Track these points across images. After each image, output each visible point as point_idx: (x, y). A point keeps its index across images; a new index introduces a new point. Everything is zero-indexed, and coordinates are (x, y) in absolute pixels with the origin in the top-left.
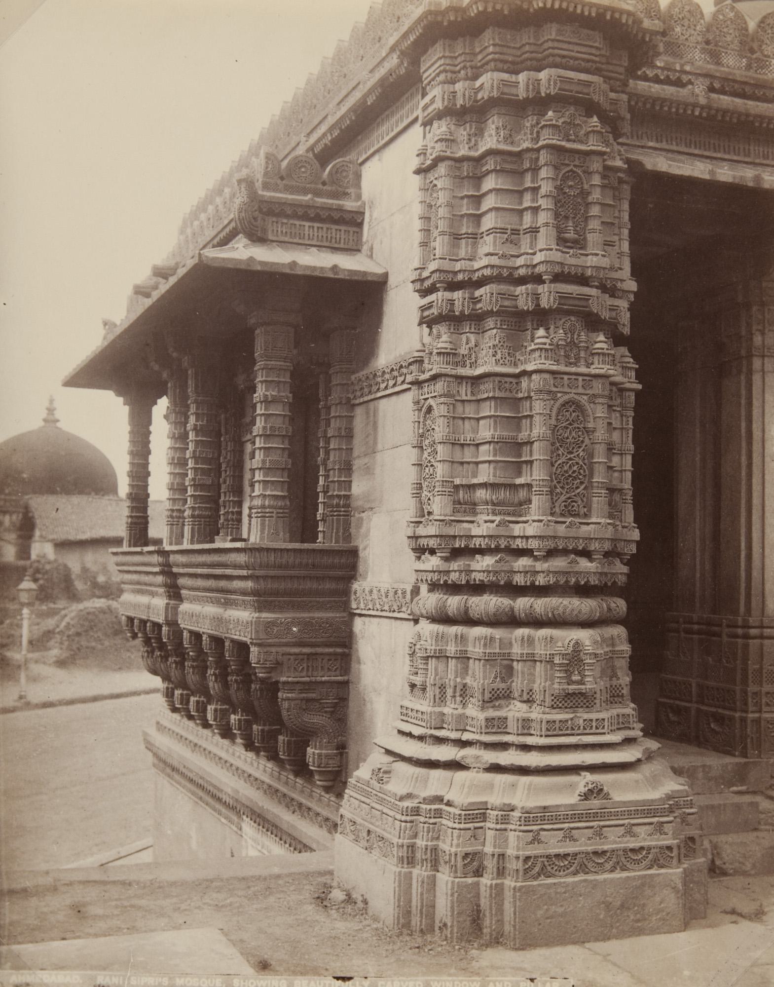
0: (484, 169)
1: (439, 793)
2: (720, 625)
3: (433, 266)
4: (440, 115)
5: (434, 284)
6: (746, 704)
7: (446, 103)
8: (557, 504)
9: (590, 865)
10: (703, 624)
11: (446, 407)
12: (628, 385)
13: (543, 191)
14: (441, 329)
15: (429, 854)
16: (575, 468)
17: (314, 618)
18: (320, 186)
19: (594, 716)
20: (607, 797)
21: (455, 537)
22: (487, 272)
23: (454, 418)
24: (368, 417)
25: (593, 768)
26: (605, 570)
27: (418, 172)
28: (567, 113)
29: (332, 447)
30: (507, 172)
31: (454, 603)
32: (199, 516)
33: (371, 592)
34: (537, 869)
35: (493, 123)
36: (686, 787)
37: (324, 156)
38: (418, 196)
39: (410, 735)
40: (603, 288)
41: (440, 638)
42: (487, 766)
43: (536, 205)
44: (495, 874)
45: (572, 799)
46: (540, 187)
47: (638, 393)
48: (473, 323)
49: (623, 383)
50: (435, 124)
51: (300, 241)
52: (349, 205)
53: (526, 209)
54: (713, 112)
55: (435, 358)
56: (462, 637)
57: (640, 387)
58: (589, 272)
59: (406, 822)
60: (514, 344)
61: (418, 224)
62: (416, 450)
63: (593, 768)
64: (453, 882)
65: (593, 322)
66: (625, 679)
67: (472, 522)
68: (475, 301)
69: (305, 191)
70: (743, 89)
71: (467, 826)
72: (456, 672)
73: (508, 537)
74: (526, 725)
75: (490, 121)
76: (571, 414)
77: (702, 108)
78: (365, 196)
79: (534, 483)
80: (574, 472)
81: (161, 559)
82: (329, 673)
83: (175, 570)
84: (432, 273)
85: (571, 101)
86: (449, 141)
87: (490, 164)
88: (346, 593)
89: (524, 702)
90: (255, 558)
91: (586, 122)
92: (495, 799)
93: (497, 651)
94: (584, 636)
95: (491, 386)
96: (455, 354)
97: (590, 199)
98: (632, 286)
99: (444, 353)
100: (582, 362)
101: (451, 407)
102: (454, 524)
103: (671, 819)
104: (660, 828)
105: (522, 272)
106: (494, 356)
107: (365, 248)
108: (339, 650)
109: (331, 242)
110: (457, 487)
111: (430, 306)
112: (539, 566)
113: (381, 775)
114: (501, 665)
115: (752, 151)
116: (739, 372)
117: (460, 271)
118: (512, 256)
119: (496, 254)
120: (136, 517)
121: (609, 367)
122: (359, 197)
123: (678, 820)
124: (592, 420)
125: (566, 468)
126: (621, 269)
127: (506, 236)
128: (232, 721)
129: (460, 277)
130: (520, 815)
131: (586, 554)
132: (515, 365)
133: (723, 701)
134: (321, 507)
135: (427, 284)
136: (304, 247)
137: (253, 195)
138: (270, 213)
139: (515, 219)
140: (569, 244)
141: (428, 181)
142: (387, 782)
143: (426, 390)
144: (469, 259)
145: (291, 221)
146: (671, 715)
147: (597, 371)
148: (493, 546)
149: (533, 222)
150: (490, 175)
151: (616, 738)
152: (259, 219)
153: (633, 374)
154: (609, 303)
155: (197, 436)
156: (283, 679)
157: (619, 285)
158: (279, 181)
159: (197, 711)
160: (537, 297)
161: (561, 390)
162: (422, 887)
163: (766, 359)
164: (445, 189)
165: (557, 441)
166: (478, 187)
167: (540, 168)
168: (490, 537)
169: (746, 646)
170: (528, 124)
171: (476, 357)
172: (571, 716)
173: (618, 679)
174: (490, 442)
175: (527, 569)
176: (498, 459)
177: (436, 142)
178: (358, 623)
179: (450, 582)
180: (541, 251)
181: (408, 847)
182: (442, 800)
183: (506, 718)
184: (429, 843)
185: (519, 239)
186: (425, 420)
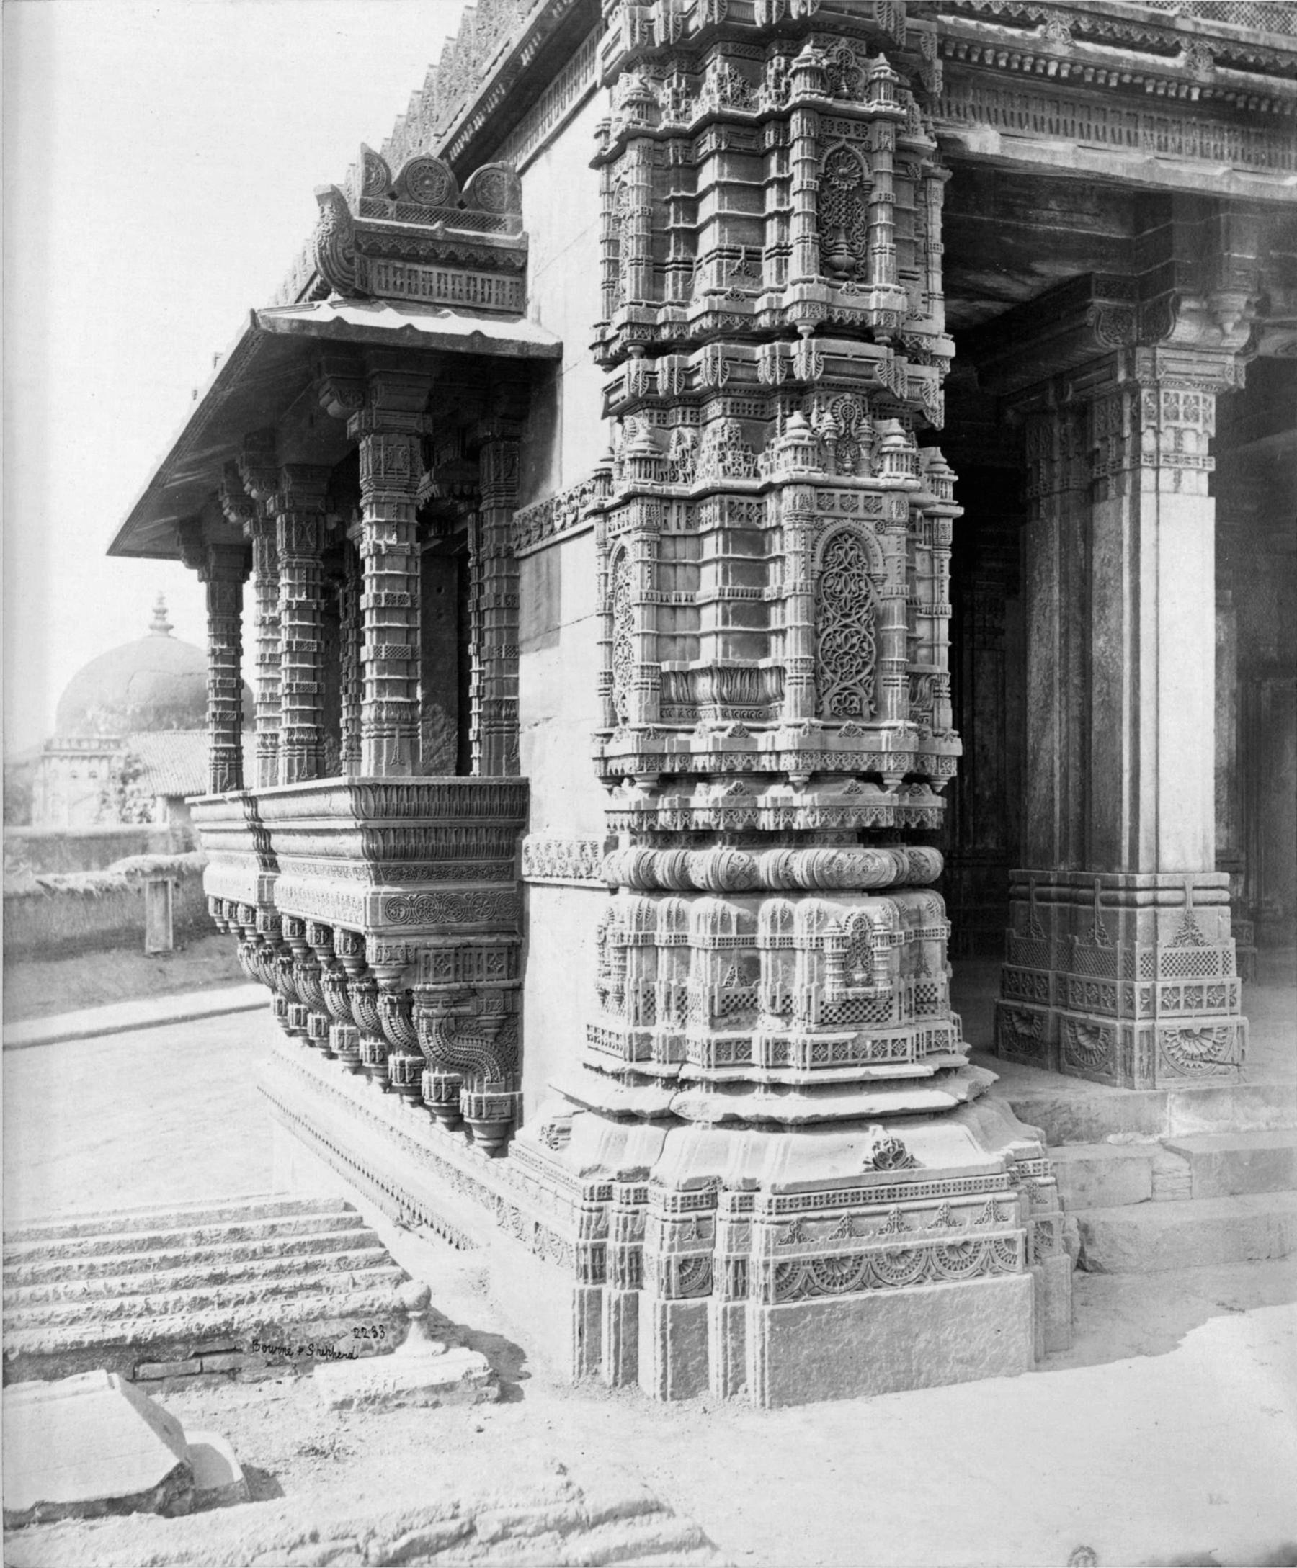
0: (702, 150)
1: (642, 1164)
2: (1092, 887)
5: (623, 349)
7: (637, 39)
8: (826, 699)
9: (883, 1274)
12: (939, 509)
13: (795, 185)
14: (637, 420)
15: (626, 1261)
16: (855, 640)
18: (456, 209)
19: (889, 1035)
20: (911, 1163)
21: (663, 755)
22: (707, 322)
24: (539, 577)
25: (886, 1118)
27: (598, 163)
28: (836, 49)
29: (487, 625)
30: (740, 153)
31: (664, 862)
32: (300, 742)
34: (798, 1284)
36: (1038, 1143)
37: (462, 167)
39: (599, 1070)
40: (898, 345)
42: (719, 1118)
43: (785, 208)
48: (689, 410)
49: (933, 504)
50: (623, 77)
51: (425, 299)
52: (499, 237)
53: (771, 216)
55: (629, 468)
56: (678, 915)
57: (960, 511)
59: (590, 1210)
60: (751, 438)
61: (600, 252)
62: (603, 619)
63: (886, 1118)
65: (880, 404)
66: (939, 977)
67: (691, 731)
69: (434, 216)
70: (1128, 33)
72: (670, 969)
73: (749, 753)
74: (778, 1051)
78: (527, 227)
79: (788, 665)
80: (853, 646)
83: (266, 826)
84: (619, 328)
86: (645, 105)
87: (710, 142)
88: (513, 850)
89: (778, 1015)
91: (866, 66)
92: (732, 1173)
93: (733, 934)
94: (877, 909)
96: (660, 461)
97: (874, 197)
98: (948, 348)
102: (662, 735)
103: (1013, 1195)
105: (764, 321)
107: (531, 309)
109: (475, 299)
110: (665, 676)
111: (617, 386)
113: (553, 1135)
114: (739, 958)
116: (1121, 493)
117: (664, 324)
118: (748, 296)
119: (722, 293)
122: (518, 226)
125: (839, 640)
127: (738, 263)
128: (362, 1050)
129: (665, 333)
131: (875, 778)
133: (1098, 1002)
134: (475, 721)
135: (615, 347)
137: (343, 221)
138: (374, 252)
140: (841, 273)
141: (613, 178)
143: (615, 521)
145: (409, 266)
147: (889, 483)
149: (781, 238)
153: (950, 490)
154: (907, 373)
155: (292, 619)
157: (925, 344)
158: (388, 201)
159: (319, 1034)
160: (787, 360)
163: (1162, 471)
168: (719, 754)
169: (1131, 919)
170: (771, 72)
171: (694, 466)
172: (854, 1035)
173: (929, 975)
174: (717, 602)
176: (730, 627)
177: (623, 108)
178: (534, 895)
180: (794, 284)
181: (593, 1250)
182: (647, 1175)
184: (627, 1245)
186: (615, 571)
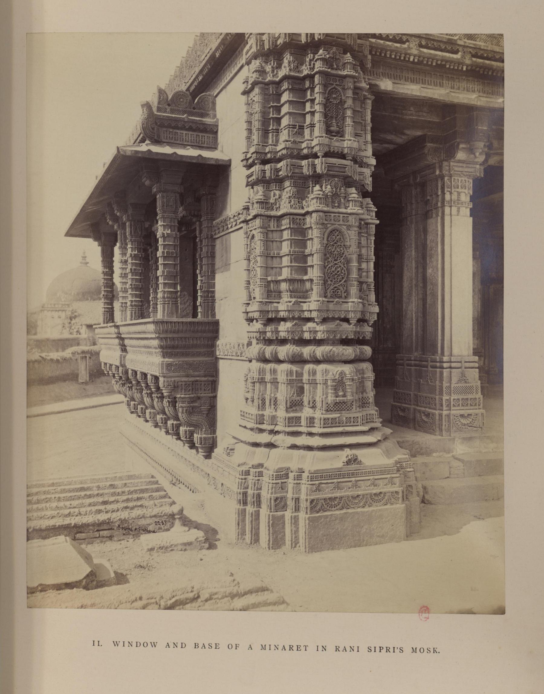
0: (282, 88)
1: (261, 462)
2: (427, 361)
3: (252, 150)
4: (255, 57)
5: (253, 162)
6: (442, 405)
7: (258, 48)
8: (328, 291)
9: (350, 504)
10: (417, 361)
11: (262, 235)
12: (370, 221)
13: (317, 101)
14: (259, 188)
16: (339, 269)
17: (194, 361)
18: (192, 110)
19: (352, 415)
20: (360, 463)
21: (268, 311)
23: (267, 241)
24: (222, 245)
25: (351, 446)
26: (358, 330)
28: (332, 51)
29: (203, 263)
30: (296, 90)
31: (269, 350)
32: (135, 305)
33: (226, 345)
34: (319, 507)
35: (287, 59)
36: (407, 456)
38: (244, 108)
39: (245, 427)
40: (355, 160)
41: (262, 372)
44: (294, 510)
45: (339, 464)
46: (315, 98)
47: (377, 226)
48: (278, 184)
49: (368, 219)
50: (253, 61)
51: (181, 143)
52: (208, 120)
53: (308, 113)
54: (421, 59)
55: (256, 205)
56: (274, 370)
57: (378, 222)
58: (346, 151)
59: (242, 479)
60: (300, 195)
61: (245, 126)
64: (269, 515)
65: (348, 182)
66: (371, 394)
67: (279, 303)
68: (278, 170)
70: (439, 46)
71: (277, 481)
72: (271, 390)
74: (311, 421)
75: (285, 59)
76: (336, 237)
77: (415, 56)
78: (218, 116)
81: (116, 330)
82: (205, 392)
83: (123, 336)
84: (252, 154)
85: (334, 43)
87: (285, 85)
88: (213, 346)
89: (311, 408)
90: (159, 327)
91: (343, 57)
92: (294, 466)
93: (294, 378)
94: (347, 369)
95: (288, 221)
96: (267, 203)
97: (346, 106)
98: (373, 162)
99: (260, 202)
100: (343, 206)
101: (265, 234)
102: (268, 304)
103: (398, 475)
104: (391, 482)
105: (305, 151)
106: (289, 203)
107: (219, 147)
108: (210, 379)
110: (269, 282)
112: (318, 328)
113: (228, 451)
114: (297, 386)
115: (445, 84)
116: (437, 215)
117: (268, 152)
118: (299, 142)
119: (290, 141)
120: (107, 308)
121: (359, 208)
122: (215, 116)
123: (402, 476)
124: (349, 241)
125: (333, 269)
126: (366, 150)
127: (296, 130)
128: (158, 419)
129: (269, 156)
130: (308, 474)
132: (303, 208)
133: (429, 404)
135: (250, 161)
136: (183, 146)
138: (162, 126)
139: (300, 119)
141: (250, 99)
142: (232, 456)
143: (250, 225)
144: (274, 145)
145: (175, 131)
146: (399, 412)
148: (291, 317)
149: (311, 121)
150: (285, 93)
151: (365, 428)
152: (156, 127)
153: (374, 214)
156: (178, 396)
157: (365, 160)
158: (167, 107)
159: (142, 413)
160: (314, 166)
161: (330, 222)
162: (252, 517)
164: (259, 102)
165: (327, 254)
166: (279, 101)
167: (315, 87)
168: (289, 311)
170: (308, 60)
171: (280, 205)
172: (339, 415)
174: (288, 255)
175: (311, 330)
176: (293, 264)
177: (253, 73)
178: (221, 362)
179: (266, 338)
180: (316, 138)
183: (300, 417)
184: (256, 492)
185: (304, 132)
186: (251, 243)
